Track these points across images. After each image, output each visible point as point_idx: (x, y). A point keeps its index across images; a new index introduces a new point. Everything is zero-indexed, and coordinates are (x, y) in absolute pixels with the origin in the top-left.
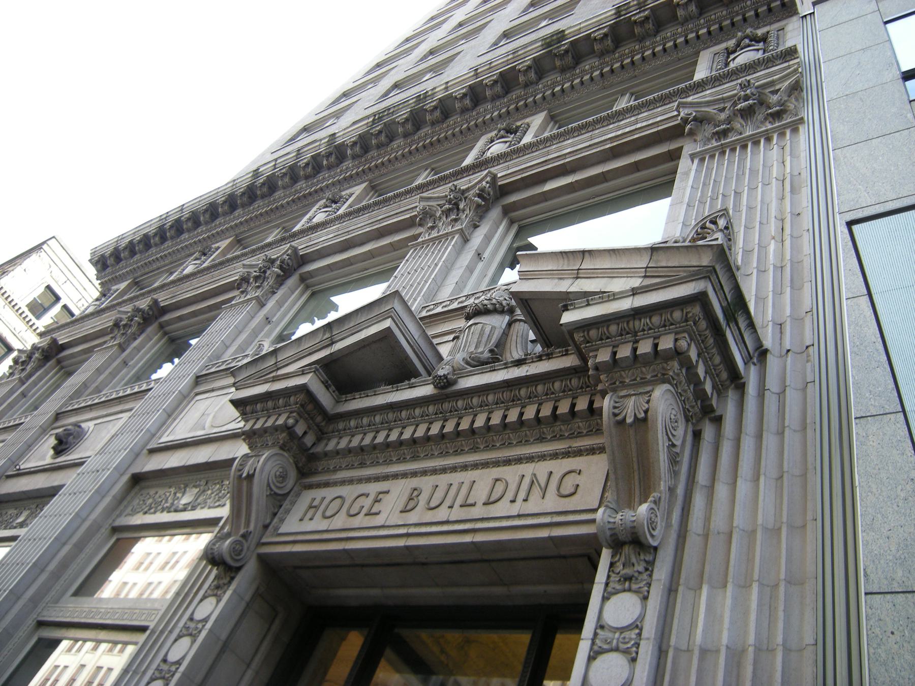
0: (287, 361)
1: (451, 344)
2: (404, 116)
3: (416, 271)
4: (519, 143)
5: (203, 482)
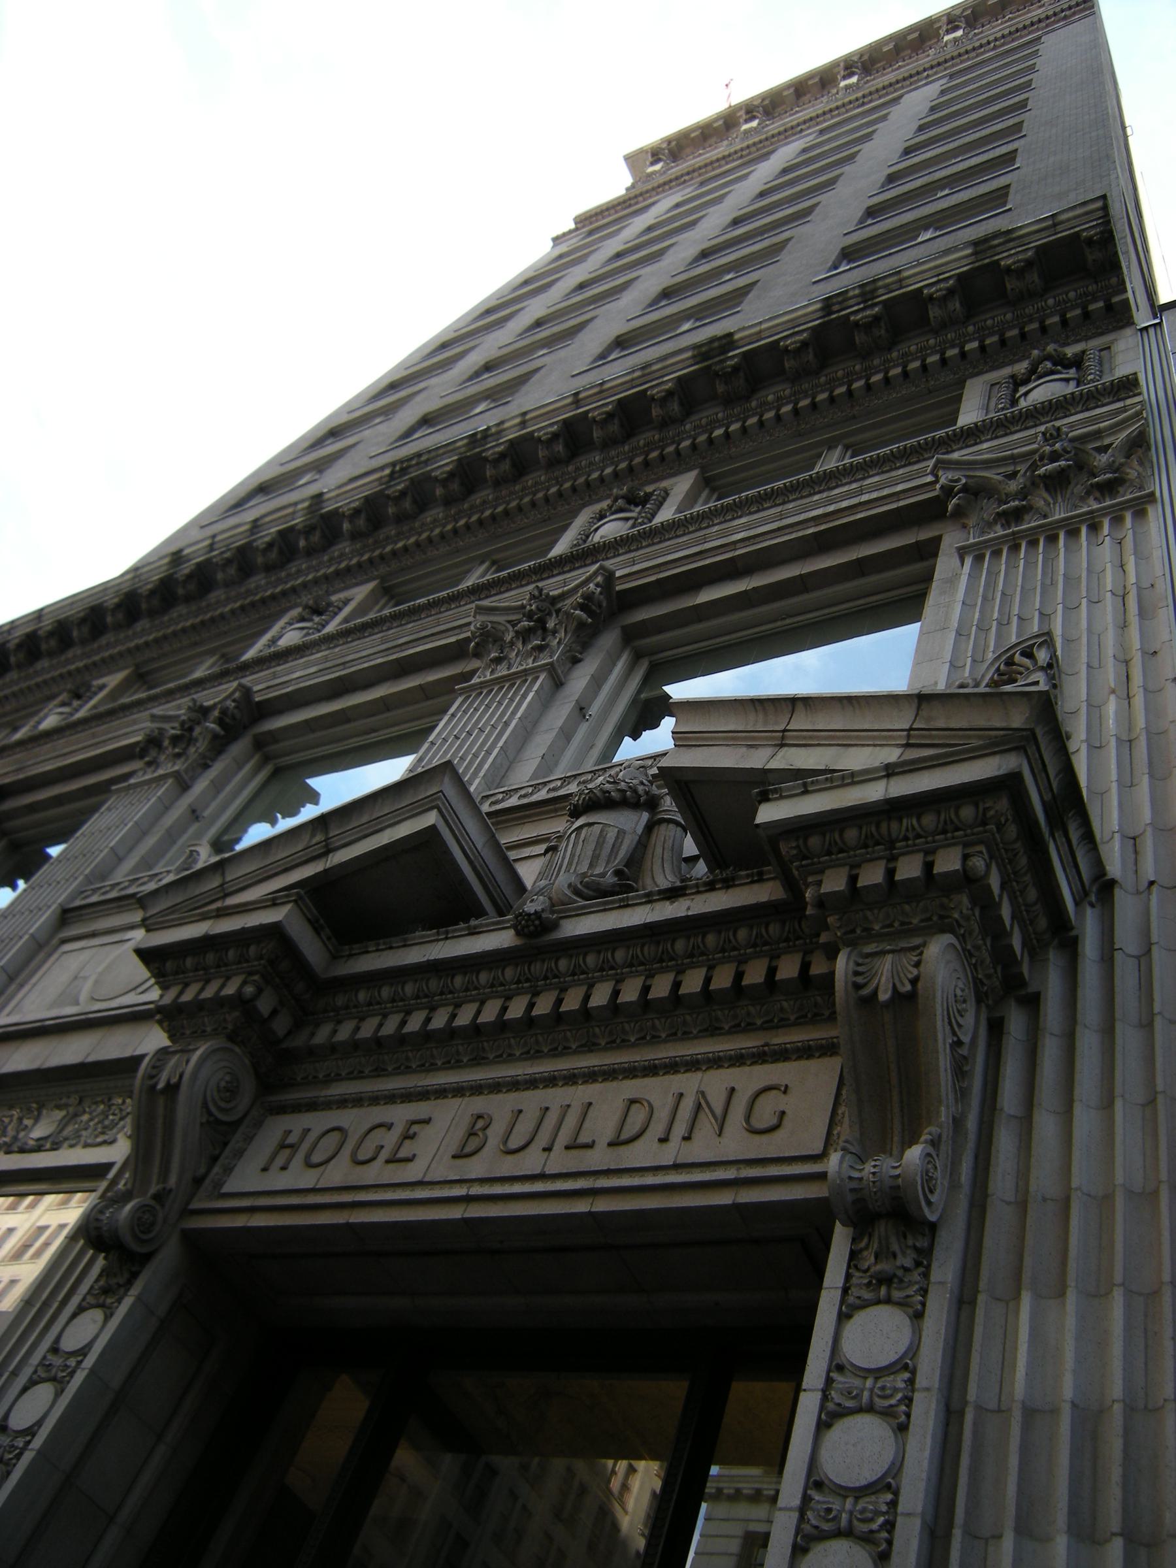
0: (244, 881)
1: (542, 860)
2: (447, 469)
3: (469, 734)
4: (650, 521)
5: (74, 1100)
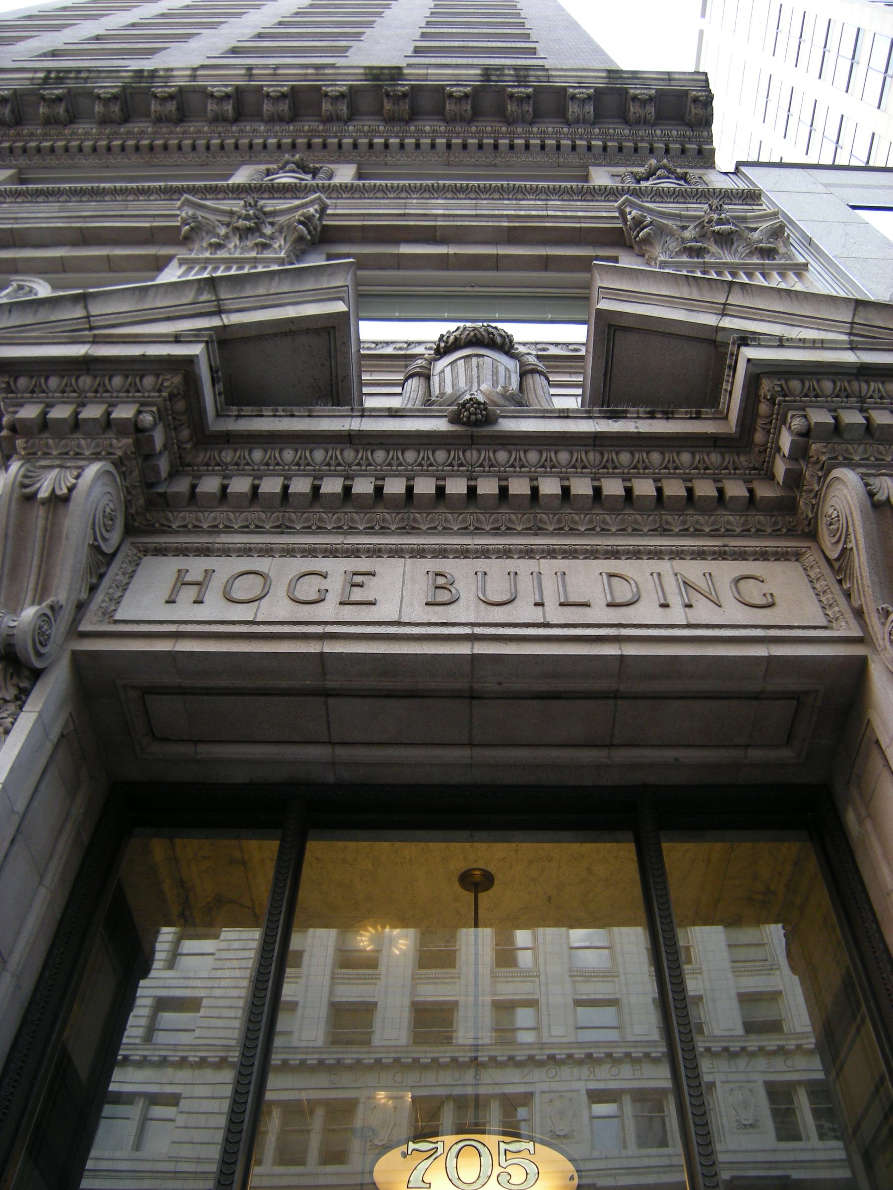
2: (113, 91)
